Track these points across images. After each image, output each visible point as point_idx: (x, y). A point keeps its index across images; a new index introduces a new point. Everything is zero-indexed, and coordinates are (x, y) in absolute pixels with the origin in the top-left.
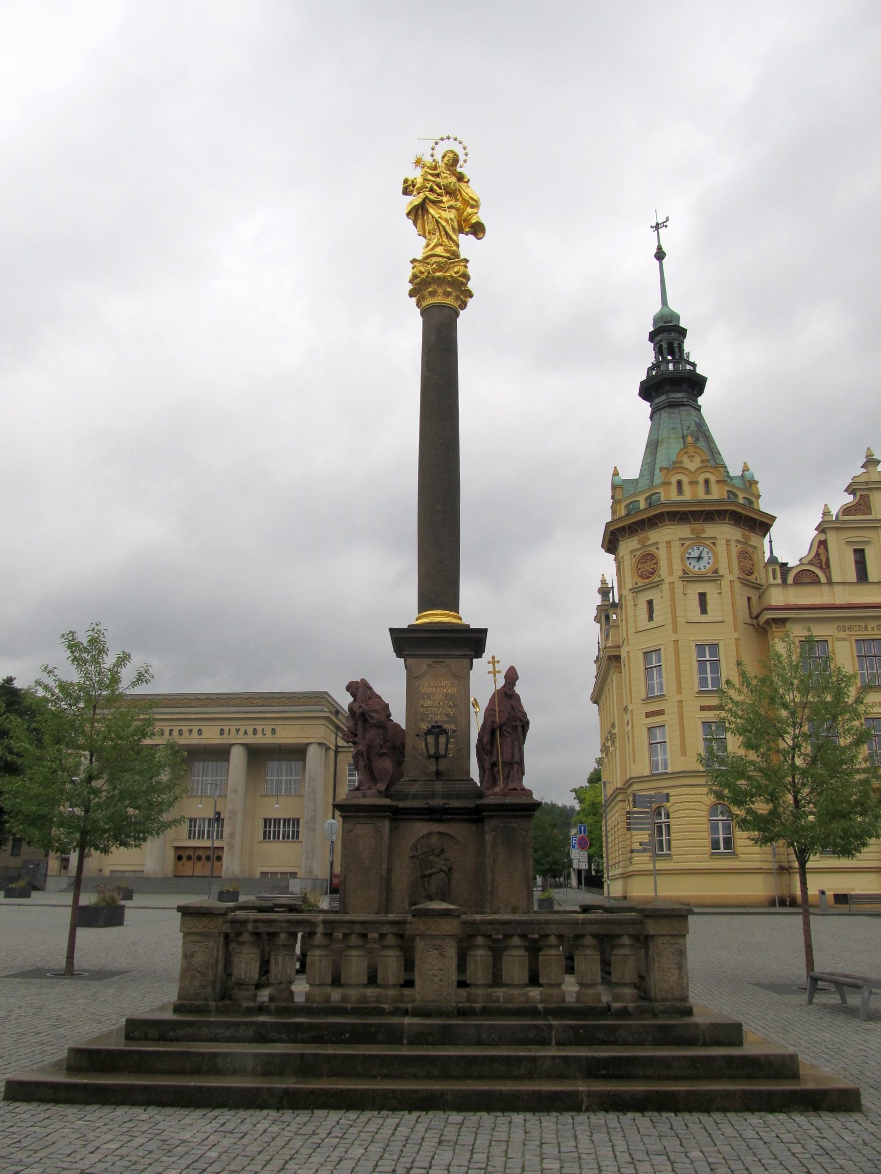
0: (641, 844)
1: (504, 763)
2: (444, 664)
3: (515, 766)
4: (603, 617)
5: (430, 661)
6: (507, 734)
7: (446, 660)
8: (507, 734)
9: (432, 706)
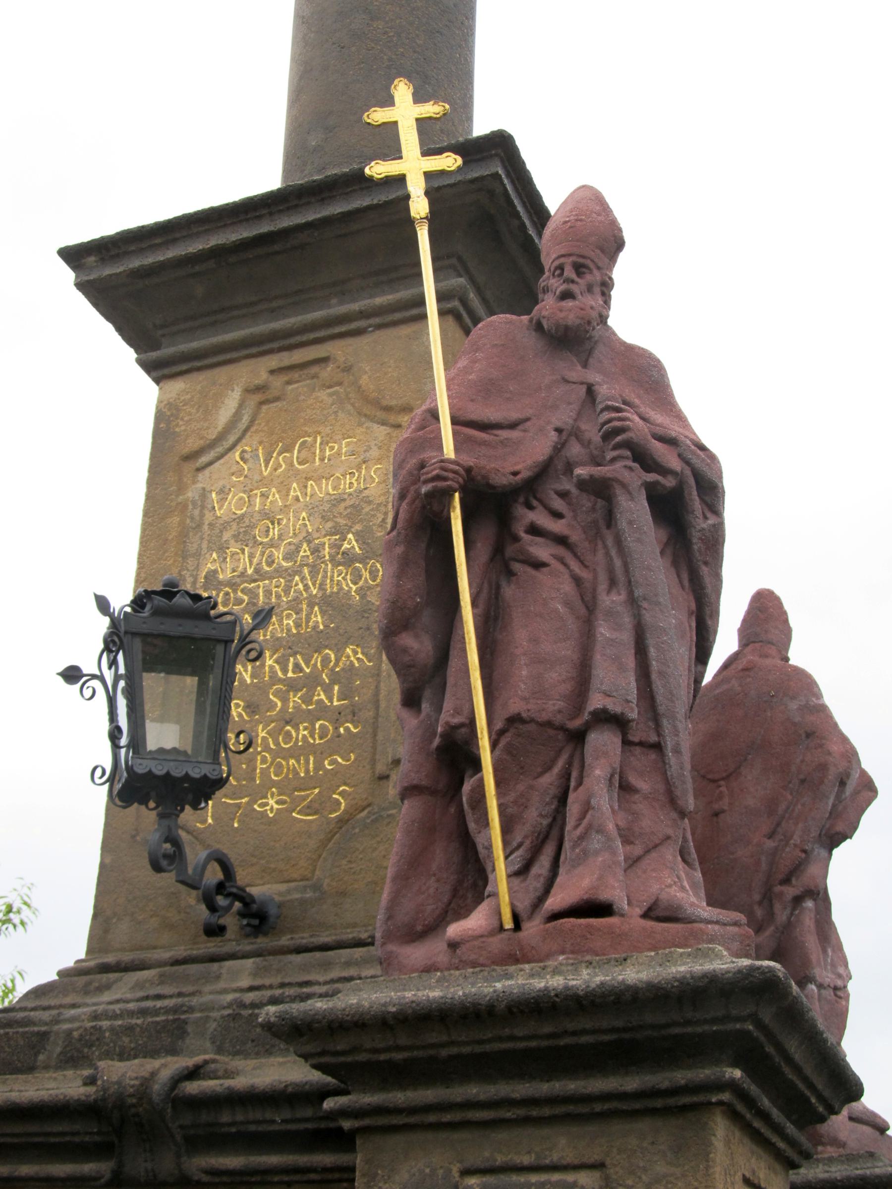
0: (771, 836)
1: (507, 728)
2: (327, 372)
3: (603, 744)
4: (849, 790)
5: (257, 370)
6: (542, 550)
7: (339, 350)
8: (542, 550)
9: (259, 574)
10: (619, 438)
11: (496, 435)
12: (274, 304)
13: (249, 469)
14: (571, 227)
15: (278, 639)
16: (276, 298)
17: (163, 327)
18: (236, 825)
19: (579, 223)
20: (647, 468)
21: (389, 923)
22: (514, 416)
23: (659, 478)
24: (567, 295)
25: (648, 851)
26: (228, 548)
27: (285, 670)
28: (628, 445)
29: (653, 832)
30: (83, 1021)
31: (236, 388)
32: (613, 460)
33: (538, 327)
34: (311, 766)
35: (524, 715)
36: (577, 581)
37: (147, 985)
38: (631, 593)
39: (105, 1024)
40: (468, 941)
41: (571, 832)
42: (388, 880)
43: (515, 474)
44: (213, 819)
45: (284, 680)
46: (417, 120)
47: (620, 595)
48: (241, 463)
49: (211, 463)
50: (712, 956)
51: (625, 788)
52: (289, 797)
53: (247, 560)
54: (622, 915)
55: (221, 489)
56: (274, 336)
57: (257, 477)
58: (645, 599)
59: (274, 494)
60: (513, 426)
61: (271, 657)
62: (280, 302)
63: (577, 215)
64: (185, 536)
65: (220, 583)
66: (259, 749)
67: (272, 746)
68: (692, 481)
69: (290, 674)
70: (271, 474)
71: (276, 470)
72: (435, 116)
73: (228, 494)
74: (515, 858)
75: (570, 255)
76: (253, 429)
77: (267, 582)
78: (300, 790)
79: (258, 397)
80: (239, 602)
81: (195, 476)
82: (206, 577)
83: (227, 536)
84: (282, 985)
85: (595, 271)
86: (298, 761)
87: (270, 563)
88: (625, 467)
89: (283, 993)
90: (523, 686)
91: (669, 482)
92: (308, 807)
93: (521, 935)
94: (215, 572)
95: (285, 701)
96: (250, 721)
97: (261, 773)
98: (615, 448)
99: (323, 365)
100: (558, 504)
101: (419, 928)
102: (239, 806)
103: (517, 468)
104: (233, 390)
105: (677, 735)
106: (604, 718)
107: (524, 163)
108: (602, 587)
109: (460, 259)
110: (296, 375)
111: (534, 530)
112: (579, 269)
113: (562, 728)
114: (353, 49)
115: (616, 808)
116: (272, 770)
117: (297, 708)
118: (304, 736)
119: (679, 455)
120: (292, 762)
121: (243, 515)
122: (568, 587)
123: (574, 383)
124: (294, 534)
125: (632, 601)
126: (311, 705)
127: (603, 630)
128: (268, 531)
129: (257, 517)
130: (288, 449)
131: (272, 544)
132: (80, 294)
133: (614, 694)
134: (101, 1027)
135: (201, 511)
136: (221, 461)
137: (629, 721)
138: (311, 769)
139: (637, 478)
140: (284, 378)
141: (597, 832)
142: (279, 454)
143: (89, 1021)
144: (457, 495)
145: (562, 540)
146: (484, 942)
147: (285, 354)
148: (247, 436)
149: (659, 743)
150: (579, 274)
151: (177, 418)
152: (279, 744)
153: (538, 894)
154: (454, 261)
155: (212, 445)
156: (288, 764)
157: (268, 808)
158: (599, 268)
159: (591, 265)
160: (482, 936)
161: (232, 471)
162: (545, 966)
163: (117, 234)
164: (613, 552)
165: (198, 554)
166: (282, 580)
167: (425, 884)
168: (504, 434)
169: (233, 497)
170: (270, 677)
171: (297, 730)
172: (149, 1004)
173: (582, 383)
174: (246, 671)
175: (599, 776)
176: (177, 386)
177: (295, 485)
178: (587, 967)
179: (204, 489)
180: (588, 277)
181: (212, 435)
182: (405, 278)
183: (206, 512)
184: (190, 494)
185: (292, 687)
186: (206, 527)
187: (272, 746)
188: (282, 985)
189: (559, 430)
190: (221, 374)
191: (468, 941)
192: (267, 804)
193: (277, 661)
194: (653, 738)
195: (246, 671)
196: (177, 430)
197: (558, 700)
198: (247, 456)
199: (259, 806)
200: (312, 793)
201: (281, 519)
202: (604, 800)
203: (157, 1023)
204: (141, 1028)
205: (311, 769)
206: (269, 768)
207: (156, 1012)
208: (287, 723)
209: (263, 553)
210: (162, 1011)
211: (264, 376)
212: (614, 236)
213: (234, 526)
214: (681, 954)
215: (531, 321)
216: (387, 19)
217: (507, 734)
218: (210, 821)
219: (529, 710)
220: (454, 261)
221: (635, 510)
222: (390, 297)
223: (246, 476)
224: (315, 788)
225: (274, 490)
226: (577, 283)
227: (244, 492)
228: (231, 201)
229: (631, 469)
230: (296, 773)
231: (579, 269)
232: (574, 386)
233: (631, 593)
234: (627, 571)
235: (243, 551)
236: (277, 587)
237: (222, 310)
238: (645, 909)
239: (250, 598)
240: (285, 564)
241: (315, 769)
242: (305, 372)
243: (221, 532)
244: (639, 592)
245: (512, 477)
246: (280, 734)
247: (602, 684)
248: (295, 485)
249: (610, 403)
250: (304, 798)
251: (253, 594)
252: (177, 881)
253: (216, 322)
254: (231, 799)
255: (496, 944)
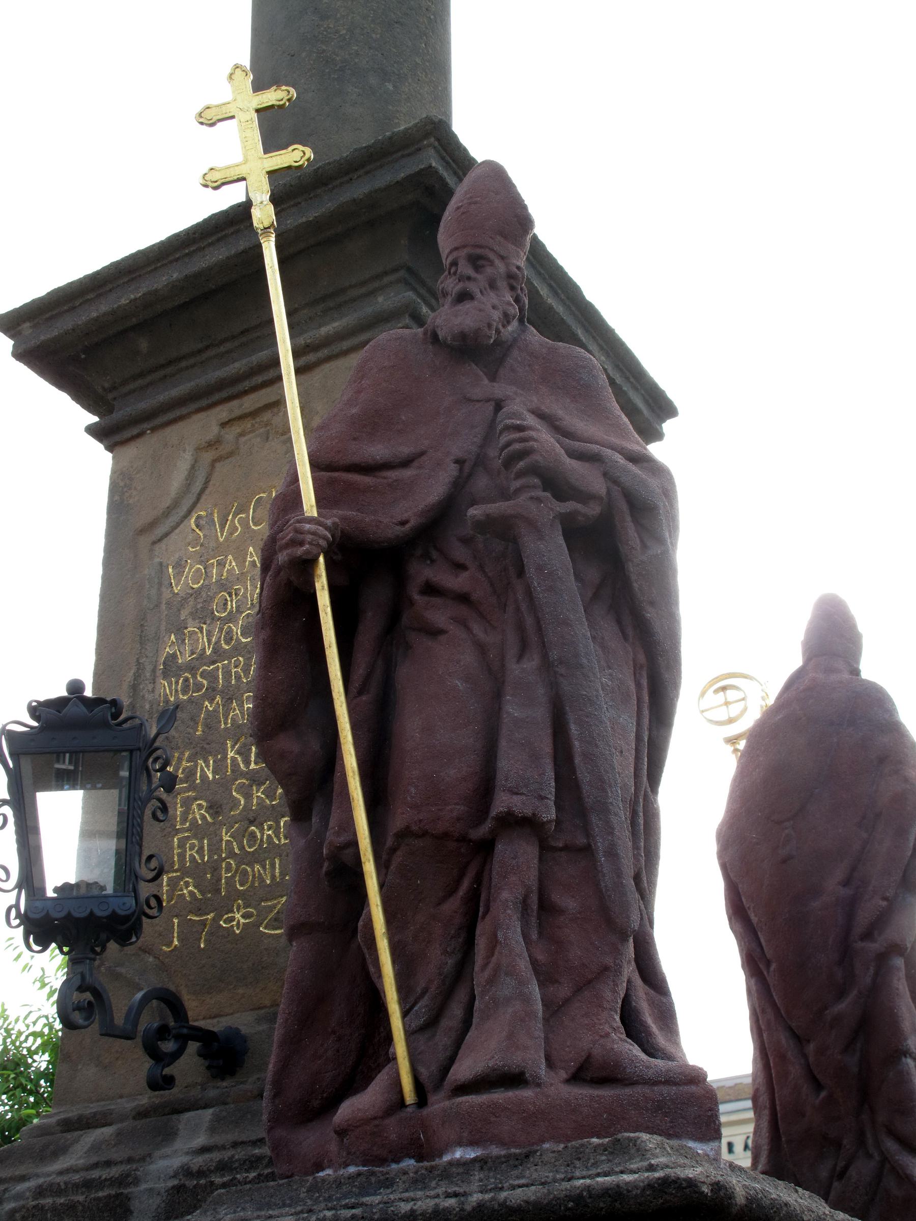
5: (202, 426)
9: (219, 654)
10: (521, 464)
11: (385, 478)
12: (222, 349)
13: (205, 536)
14: (463, 213)
15: (239, 726)
16: (222, 342)
17: (114, 388)
18: (202, 946)
19: (473, 206)
20: (560, 496)
21: (277, 1102)
22: (405, 450)
23: (579, 506)
24: (464, 297)
25: (579, 990)
26: (186, 628)
27: (247, 763)
28: (534, 470)
29: (583, 964)
30: (28, 1198)
31: (187, 448)
32: (518, 491)
33: (434, 338)
34: (277, 871)
35: (414, 828)
36: (482, 648)
37: (103, 1147)
38: (545, 656)
39: (48, 1201)
40: (357, 1127)
41: (480, 977)
42: (275, 1045)
43: (403, 523)
44: (178, 941)
45: (247, 773)
46: (258, 111)
47: (533, 660)
48: (197, 530)
49: (167, 535)
50: (633, 1151)
51: (546, 908)
52: (255, 909)
53: (205, 640)
54: (539, 1085)
55: (177, 563)
56: (221, 385)
57: (213, 544)
58: (561, 663)
59: (231, 562)
60: (406, 463)
61: (233, 747)
62: (228, 346)
63: (471, 197)
64: (143, 620)
65: (180, 668)
66: (224, 855)
67: (237, 851)
68: (623, 505)
69: (253, 766)
70: (227, 539)
71: (232, 534)
72: (278, 103)
73: (185, 567)
74: (420, 1008)
75: (464, 246)
76: (207, 492)
77: (226, 662)
78: (267, 900)
79: (208, 456)
80: (199, 687)
81: (151, 550)
82: (164, 663)
83: (184, 614)
84: (235, 1145)
85: (497, 262)
86: (264, 867)
87: (228, 640)
88: (532, 498)
89: (233, 1156)
90: (413, 790)
91: (593, 510)
92: (276, 919)
93: (425, 1111)
94: (174, 656)
95: (248, 796)
96: (214, 823)
97: (226, 883)
98: (519, 475)
99: (275, 410)
100: (460, 553)
101: (316, 1103)
102: (203, 923)
103: (405, 516)
104: (184, 451)
105: (612, 833)
106: (513, 823)
107: (465, 150)
108: (512, 652)
109: (410, 270)
110: (248, 424)
111: (431, 589)
112: (477, 262)
113: (463, 839)
114: (304, 54)
115: (534, 936)
116: (237, 878)
117: (261, 802)
118: (269, 836)
119: (605, 474)
120: (257, 867)
121: (200, 588)
122: (468, 657)
123: (478, 401)
124: (252, 604)
125: (547, 665)
126: (275, 799)
127: (512, 709)
128: (226, 604)
129: (214, 588)
130: (243, 509)
131: (231, 618)
132: (22, 365)
133: (524, 790)
134: (43, 1206)
135: (159, 589)
136: (177, 531)
137: (543, 824)
138: (277, 875)
139: (546, 510)
140: (236, 429)
141: (506, 974)
142: (234, 517)
143: (35, 1199)
144: (321, 559)
145: (463, 598)
146: (377, 1126)
147: (235, 403)
148: (202, 500)
149: (589, 845)
150: (477, 269)
151: (130, 489)
152: (244, 848)
153: (448, 1054)
154: (402, 273)
155: (167, 513)
156: (253, 871)
157: (234, 923)
158: (502, 258)
159: (491, 256)
160: (375, 1118)
161: (188, 540)
162: (432, 1167)
163: (48, 294)
164: (524, 607)
165: (157, 638)
166: (241, 659)
167: (322, 1045)
168: (393, 475)
169: (190, 569)
170: (233, 771)
171: (262, 831)
172: (95, 1174)
173: (488, 400)
174: (208, 766)
175: (507, 900)
176: (131, 451)
177: (251, 549)
178: (482, 1168)
179: (161, 564)
180: (489, 270)
181: (168, 502)
182: (354, 300)
183: (164, 589)
184: (146, 572)
185: (254, 781)
186: (163, 607)
187: (237, 851)
188: (235, 1145)
189: (459, 462)
190: (172, 433)
191: (357, 1127)
192: (232, 919)
193: (238, 752)
194: (581, 841)
195: (208, 766)
196: (131, 501)
197: (457, 804)
198: (202, 522)
199: (225, 922)
200: (279, 903)
201: (239, 589)
202: (513, 933)
203: (99, 1199)
204: (83, 1206)
205: (277, 875)
206: (233, 876)
207: (100, 1184)
208: (252, 822)
209: (221, 629)
210: (107, 1183)
211: (215, 429)
212: (517, 216)
213: (191, 602)
214: (596, 1148)
215: (425, 333)
216: (338, 15)
217: (399, 853)
218: (176, 942)
219: (420, 821)
220: (402, 273)
221: (549, 552)
222: (336, 324)
223: (202, 545)
224: (282, 897)
225: (230, 557)
226: (475, 280)
227: (201, 563)
228: (158, 241)
229: (538, 500)
230: (262, 881)
231: (477, 262)
232: (478, 405)
233: (545, 656)
234: (539, 629)
235: (201, 629)
236: (236, 667)
237: (170, 363)
238: (573, 1070)
239: (209, 682)
240: (244, 640)
241: (281, 873)
242: (258, 420)
243: (179, 610)
244: (554, 654)
245: (398, 528)
246: (244, 836)
247: (506, 780)
248: (251, 549)
249: (509, 422)
250: (274, 906)
251: (211, 677)
252: (101, 1035)
253: (165, 376)
254: (196, 915)
255: (393, 1129)
